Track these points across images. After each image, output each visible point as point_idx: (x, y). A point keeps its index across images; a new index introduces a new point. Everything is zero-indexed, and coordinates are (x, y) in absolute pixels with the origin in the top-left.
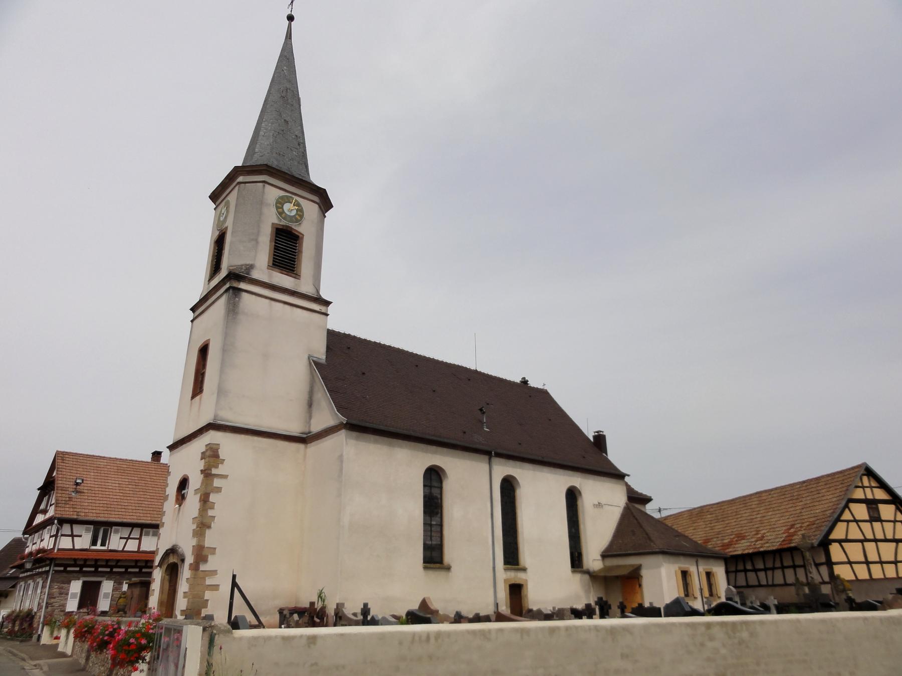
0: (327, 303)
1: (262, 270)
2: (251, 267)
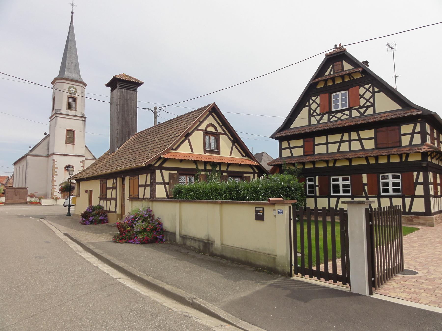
0: (85, 118)
1: (64, 110)
2: (60, 110)
